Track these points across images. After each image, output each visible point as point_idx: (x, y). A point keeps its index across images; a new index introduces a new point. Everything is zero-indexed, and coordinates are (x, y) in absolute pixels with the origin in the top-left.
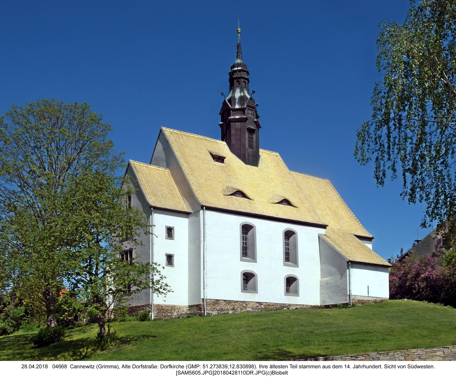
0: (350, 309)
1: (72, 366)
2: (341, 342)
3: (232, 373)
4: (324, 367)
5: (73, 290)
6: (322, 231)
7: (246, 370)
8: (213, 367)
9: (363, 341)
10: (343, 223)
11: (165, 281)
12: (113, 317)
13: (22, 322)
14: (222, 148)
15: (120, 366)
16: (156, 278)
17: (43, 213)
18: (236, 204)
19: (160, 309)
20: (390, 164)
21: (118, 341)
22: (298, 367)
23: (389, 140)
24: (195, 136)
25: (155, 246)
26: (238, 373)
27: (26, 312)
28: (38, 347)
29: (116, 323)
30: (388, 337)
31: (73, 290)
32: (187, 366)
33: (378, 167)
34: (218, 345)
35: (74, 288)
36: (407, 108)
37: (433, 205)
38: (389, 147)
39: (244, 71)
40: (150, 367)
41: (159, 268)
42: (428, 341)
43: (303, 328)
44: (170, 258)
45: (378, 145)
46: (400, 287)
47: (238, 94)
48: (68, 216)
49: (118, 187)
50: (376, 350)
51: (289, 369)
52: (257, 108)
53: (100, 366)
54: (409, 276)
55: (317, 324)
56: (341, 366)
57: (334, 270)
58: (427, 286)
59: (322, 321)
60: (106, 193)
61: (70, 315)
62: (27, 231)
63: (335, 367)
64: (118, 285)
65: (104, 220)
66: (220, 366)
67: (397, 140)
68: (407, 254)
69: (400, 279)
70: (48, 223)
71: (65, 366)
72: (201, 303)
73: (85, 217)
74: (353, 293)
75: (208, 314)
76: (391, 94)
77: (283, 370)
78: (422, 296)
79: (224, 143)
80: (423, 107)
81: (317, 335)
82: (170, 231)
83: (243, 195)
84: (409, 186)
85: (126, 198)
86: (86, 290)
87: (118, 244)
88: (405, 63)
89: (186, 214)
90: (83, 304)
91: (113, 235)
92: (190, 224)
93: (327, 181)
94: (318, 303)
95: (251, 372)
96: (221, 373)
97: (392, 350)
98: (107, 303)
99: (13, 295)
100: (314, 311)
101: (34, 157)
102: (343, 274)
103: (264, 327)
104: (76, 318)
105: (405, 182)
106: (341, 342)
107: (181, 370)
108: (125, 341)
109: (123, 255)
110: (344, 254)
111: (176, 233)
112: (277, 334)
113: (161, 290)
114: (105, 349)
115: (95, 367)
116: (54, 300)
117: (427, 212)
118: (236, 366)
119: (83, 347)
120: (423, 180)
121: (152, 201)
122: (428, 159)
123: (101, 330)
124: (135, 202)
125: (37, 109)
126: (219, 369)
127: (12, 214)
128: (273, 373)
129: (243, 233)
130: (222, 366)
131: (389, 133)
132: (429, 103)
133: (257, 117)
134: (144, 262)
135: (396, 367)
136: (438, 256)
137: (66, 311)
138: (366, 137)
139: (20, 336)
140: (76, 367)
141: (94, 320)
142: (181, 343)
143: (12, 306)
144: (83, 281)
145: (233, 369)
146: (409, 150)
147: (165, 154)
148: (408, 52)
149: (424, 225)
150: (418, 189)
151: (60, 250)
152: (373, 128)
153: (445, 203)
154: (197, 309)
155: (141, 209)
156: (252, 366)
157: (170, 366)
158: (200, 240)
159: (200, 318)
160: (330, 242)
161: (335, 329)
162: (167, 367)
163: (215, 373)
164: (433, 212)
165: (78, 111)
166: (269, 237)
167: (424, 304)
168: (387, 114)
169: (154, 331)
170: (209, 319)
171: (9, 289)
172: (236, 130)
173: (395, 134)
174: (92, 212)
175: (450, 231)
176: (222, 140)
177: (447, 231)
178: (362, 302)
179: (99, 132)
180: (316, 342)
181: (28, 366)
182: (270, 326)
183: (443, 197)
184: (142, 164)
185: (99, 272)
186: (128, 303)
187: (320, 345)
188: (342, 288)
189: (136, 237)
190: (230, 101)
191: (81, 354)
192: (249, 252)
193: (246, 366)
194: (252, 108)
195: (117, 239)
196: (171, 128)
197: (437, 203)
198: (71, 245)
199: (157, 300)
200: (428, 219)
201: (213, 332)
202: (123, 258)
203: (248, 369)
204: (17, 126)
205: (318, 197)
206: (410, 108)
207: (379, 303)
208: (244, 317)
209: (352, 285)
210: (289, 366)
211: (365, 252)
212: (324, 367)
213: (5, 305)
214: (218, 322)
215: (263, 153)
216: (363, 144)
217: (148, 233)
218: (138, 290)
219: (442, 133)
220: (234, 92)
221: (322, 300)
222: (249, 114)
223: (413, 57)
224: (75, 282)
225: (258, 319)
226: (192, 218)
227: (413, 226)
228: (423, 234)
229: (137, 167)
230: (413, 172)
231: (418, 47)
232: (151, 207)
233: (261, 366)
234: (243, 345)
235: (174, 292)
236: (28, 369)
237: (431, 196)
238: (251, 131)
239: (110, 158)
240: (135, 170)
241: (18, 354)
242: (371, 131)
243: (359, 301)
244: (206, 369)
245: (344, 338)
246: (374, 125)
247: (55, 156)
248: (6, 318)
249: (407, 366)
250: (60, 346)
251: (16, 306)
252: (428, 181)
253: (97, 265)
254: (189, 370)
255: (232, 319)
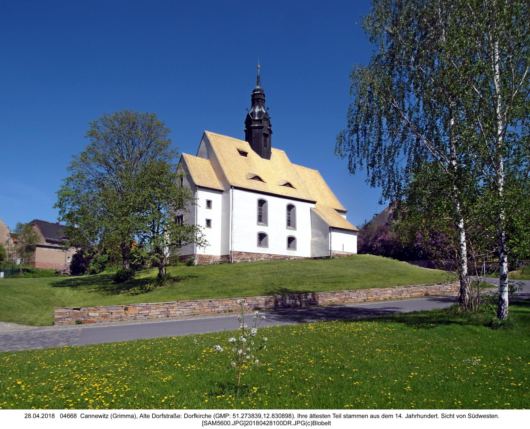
0: (331, 260)
1: (83, 416)
2: (324, 282)
3: (266, 423)
4: (372, 416)
5: (141, 243)
6: (313, 206)
7: (282, 419)
8: (244, 417)
9: (339, 282)
10: (327, 200)
11: (204, 238)
12: (168, 263)
13: (106, 265)
14: (246, 146)
15: (138, 416)
16: (199, 235)
17: (122, 189)
18: (255, 186)
19: (201, 257)
20: (358, 159)
21: (172, 280)
22: (342, 416)
23: (358, 144)
24: (228, 137)
25: (198, 213)
26: (273, 423)
27: (109, 259)
28: (116, 283)
29: (171, 267)
30: (356, 280)
31: (141, 243)
32: (215, 416)
33: (350, 162)
34: (241, 284)
35: (142, 241)
36: (370, 122)
37: (386, 189)
38: (358, 148)
39: (262, 94)
40: (172, 417)
41: (201, 229)
42: (382, 283)
43: (299, 273)
44: (208, 222)
45: (351, 146)
46: (365, 246)
47: (257, 110)
48: (139, 191)
49: (174, 172)
50: (347, 289)
51: (332, 419)
52: (270, 120)
53: (115, 415)
54: (370, 238)
55: (309, 270)
56: (391, 416)
57: (320, 233)
58: (382, 246)
59: (312, 268)
60: (166, 176)
61: (138, 261)
62: (110, 201)
63: (384, 416)
64: (172, 240)
65: (164, 194)
66: (253, 415)
67: (363, 143)
68: (369, 224)
69: (364, 240)
70: (125, 196)
71: (75, 416)
72: (230, 254)
73: (150, 192)
74: (333, 249)
75: (234, 262)
76: (360, 112)
77: (325, 420)
78: (379, 252)
79: (247, 143)
80: (380, 122)
81: (308, 277)
82: (209, 203)
83: (260, 179)
84: (371, 176)
85: (178, 179)
86: (150, 244)
87: (173, 212)
88: (369, 92)
89: (221, 192)
90: (147, 253)
91: (170, 205)
92: (223, 199)
93: (317, 171)
94: (309, 256)
95: (289, 423)
96: (253, 423)
97: (358, 289)
98: (165, 253)
99: (100, 246)
100: (307, 261)
101: (117, 150)
102: (326, 236)
103: (272, 271)
104: (143, 263)
105: (368, 173)
106: (324, 282)
107: (208, 420)
108: (176, 280)
109: (176, 220)
110: (327, 222)
111: (213, 204)
112: (281, 276)
113: (202, 244)
114: (163, 285)
115: (109, 416)
116: (128, 250)
117: (383, 194)
118: (271, 416)
119: (147, 283)
120: (380, 172)
121: (197, 182)
122: (383, 158)
123: (160, 271)
124: (185, 182)
125: (120, 117)
126: (251, 419)
127: (101, 189)
128: (314, 423)
129: (259, 206)
130: (255, 416)
131: (358, 138)
132: (384, 120)
133: (270, 126)
134: (191, 225)
135: (455, 416)
136: (389, 225)
137: (136, 258)
138: (343, 141)
139: (104, 275)
140: (87, 416)
141: (155, 264)
142: (215, 282)
143: (98, 254)
144: (148, 237)
145: (268, 419)
146: (370, 151)
147: (207, 149)
148: (371, 84)
149: (380, 203)
150: (377, 178)
151: (133, 215)
152: (347, 135)
153: (395, 188)
154: (227, 258)
155: (189, 187)
156: (289, 416)
157: (196, 416)
158: (229, 208)
159: (229, 264)
160: (318, 213)
161: (320, 274)
162: (192, 416)
163: (246, 423)
164: (386, 194)
165: (148, 118)
166: (277, 208)
167: (380, 258)
168: (357, 126)
169: (196, 273)
170: (235, 265)
171: (97, 242)
172: (255, 134)
173: (362, 139)
174: (156, 188)
175: (397, 207)
176: (246, 141)
177: (396, 207)
178: (339, 256)
179: (162, 133)
180: (308, 283)
181: (32, 416)
182: (276, 271)
183: (393, 184)
184: (191, 156)
185: (159, 231)
186: (179, 253)
187: (310, 285)
188: (326, 245)
189: (186, 207)
190: (252, 114)
191: (146, 289)
192: (263, 219)
193: (283, 416)
194: (267, 119)
195: (173, 208)
196: (211, 131)
197: (389, 188)
198: (140, 212)
199: (199, 251)
200: (383, 198)
201: (237, 275)
202: (176, 221)
203: (285, 419)
204: (106, 128)
205: (310, 182)
206: (372, 122)
207: (350, 257)
208: (259, 264)
209: (332, 244)
210: (332, 416)
211: (341, 221)
212: (372, 416)
213: (94, 253)
214: (241, 267)
215: (274, 151)
216: (340, 145)
217: (194, 204)
218: (186, 244)
219: (393, 140)
220: (255, 108)
221: (312, 254)
222: (265, 124)
223: (374, 88)
224: (142, 237)
225: (268, 266)
226: (225, 194)
227: (375, 204)
228: (380, 209)
229: (187, 158)
230: (372, 166)
231: (377, 82)
232: (196, 186)
233: (299, 416)
234: (257, 284)
235: (210, 246)
236: (32, 419)
237: (385, 183)
238: (266, 136)
239: (169, 151)
240: (186, 160)
241: (103, 288)
242: (346, 137)
243: (337, 255)
244: (236, 419)
245: (326, 280)
246: (348, 132)
247: (131, 149)
248: (95, 263)
249: (467, 416)
250: (132, 283)
251: (102, 254)
252: (383, 173)
253: (158, 226)
254: (217, 420)
255: (251, 266)
